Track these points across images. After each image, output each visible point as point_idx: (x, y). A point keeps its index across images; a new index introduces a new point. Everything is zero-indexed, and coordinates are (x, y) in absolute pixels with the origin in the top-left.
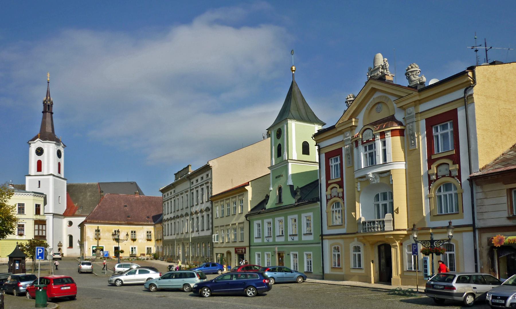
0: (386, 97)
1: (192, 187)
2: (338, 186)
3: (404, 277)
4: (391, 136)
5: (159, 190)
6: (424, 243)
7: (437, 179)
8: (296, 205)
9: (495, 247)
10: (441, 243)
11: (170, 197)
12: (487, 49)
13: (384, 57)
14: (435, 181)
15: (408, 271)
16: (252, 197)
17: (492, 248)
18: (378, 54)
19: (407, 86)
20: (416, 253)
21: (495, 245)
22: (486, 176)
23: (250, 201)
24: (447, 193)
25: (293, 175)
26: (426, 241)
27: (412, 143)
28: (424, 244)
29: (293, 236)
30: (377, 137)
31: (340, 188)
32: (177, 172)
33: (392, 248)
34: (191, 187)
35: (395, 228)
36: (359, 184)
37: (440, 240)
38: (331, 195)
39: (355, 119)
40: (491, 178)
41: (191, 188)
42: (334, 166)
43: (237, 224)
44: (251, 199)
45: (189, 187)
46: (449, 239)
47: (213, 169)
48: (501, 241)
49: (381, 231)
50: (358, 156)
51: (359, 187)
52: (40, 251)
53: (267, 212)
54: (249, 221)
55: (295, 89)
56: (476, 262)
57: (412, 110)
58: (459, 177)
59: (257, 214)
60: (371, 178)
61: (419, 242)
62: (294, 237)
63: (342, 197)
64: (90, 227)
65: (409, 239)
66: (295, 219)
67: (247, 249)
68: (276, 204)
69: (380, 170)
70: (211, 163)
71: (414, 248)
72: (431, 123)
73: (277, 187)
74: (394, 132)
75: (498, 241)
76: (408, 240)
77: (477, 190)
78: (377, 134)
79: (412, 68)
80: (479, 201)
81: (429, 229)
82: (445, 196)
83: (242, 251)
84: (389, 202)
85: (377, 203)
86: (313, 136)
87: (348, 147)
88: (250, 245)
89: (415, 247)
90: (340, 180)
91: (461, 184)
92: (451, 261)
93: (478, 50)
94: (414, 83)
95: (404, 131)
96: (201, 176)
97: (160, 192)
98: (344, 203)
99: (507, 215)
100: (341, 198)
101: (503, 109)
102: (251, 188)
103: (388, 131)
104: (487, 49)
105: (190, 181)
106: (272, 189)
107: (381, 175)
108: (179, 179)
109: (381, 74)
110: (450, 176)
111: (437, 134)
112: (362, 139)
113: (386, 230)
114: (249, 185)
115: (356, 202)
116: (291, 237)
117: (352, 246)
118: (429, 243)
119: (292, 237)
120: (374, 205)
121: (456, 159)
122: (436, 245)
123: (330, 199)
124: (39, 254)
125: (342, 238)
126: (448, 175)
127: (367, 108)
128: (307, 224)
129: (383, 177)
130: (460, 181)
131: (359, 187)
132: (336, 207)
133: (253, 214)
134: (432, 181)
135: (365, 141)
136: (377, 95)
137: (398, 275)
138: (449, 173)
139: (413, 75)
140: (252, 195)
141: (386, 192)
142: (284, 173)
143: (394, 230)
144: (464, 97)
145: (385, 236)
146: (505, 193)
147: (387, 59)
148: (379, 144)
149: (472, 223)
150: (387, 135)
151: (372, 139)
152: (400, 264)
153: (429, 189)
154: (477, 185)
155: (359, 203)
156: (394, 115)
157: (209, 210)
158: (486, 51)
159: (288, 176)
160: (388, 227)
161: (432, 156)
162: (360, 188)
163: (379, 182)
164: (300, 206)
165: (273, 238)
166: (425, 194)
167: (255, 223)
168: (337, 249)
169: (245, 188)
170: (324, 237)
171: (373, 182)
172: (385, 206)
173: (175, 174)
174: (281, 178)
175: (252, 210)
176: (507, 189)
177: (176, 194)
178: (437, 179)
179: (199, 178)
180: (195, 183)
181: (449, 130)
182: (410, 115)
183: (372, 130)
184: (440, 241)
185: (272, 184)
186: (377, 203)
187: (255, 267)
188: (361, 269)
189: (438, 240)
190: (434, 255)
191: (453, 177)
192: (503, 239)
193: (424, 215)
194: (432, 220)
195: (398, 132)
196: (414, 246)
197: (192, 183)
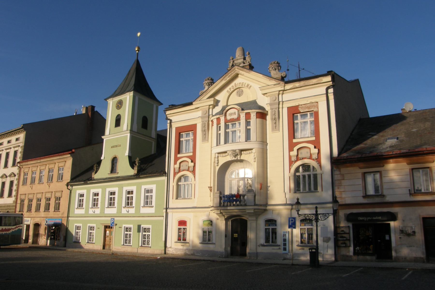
2: (189, 161)
10: (327, 216)
37: (326, 214)
50: (275, 127)
61: (302, 216)
62: (128, 209)
63: (316, 159)
64: (301, 132)
66: (83, 193)
71: (291, 222)
89: (112, 220)
90: (191, 154)
93: (287, 70)
96: (17, 136)
98: (195, 177)
99: (362, 195)
110: (310, 158)
119: (127, 209)
122: (321, 218)
123: (295, 161)
124: (292, 223)
125: (193, 212)
128: (80, 201)
146: (360, 175)
156: (256, 100)
157: (15, 176)
176: (362, 173)
181: (191, 137)
184: (326, 215)
188: (93, 243)
189: (323, 214)
196: (112, 219)
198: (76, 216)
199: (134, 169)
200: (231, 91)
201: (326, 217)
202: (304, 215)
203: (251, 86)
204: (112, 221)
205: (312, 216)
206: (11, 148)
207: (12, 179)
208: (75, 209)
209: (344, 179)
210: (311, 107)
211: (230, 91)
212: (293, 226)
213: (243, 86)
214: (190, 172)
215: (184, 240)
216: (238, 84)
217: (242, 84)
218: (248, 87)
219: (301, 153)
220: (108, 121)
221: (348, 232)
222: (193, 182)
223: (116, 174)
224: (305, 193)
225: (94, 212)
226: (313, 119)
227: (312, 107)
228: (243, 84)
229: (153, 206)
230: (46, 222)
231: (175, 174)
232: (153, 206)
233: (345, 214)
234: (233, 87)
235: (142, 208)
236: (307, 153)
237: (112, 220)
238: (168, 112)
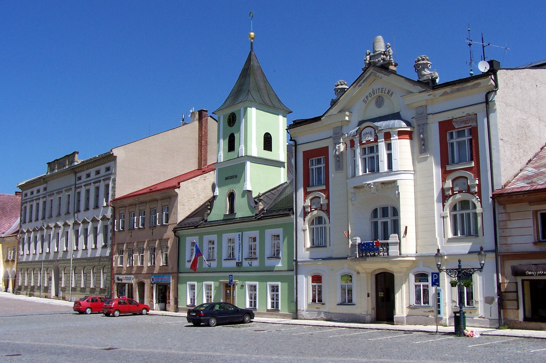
1: (78, 184)
4: (398, 139)
5: (17, 186)
6: (450, 272)
11: (36, 197)
12: (484, 46)
13: (385, 42)
18: (377, 37)
19: (416, 81)
20: (438, 284)
22: (510, 195)
24: (465, 212)
26: (452, 269)
28: (450, 274)
32: (53, 161)
34: (76, 184)
35: (402, 252)
37: (470, 269)
39: (349, 112)
40: (508, 198)
41: (77, 186)
42: (315, 168)
45: (74, 183)
46: (480, 267)
47: (118, 160)
52: (435, 276)
55: (254, 63)
59: (193, 227)
62: (251, 261)
70: (115, 152)
71: (434, 278)
80: (502, 224)
82: (462, 215)
84: (391, 220)
85: (375, 220)
86: (288, 128)
89: (231, 278)
94: (425, 78)
95: (412, 133)
97: (18, 188)
98: (329, 218)
99: (533, 241)
101: (520, 119)
104: (484, 46)
105: (76, 176)
108: (56, 171)
109: (382, 61)
111: (452, 141)
116: (248, 261)
118: (456, 272)
119: (250, 262)
120: (370, 222)
126: (466, 191)
132: (317, 223)
133: (181, 229)
134: (447, 196)
135: (365, 142)
138: (467, 188)
141: (388, 207)
147: (390, 43)
148: (382, 146)
152: (406, 298)
153: (444, 206)
156: (399, 112)
158: (483, 47)
164: (264, 219)
165: (217, 262)
172: (385, 224)
173: (47, 163)
176: (533, 211)
177: (47, 193)
179: (93, 171)
180: (84, 179)
186: (375, 220)
187: (434, 281)
189: (468, 269)
191: (472, 194)
196: (434, 275)
197: (80, 178)
198: (212, 271)
200: (368, 100)
202: (445, 270)
203: (392, 93)
204: (230, 279)
205: (455, 272)
206: (100, 181)
207: (105, 223)
208: (186, 262)
209: (509, 220)
210: (468, 120)
211: (367, 100)
213: (382, 93)
214: (323, 211)
215: (320, 301)
216: (376, 90)
217: (382, 91)
218: (389, 95)
220: (284, 136)
221: (515, 290)
222: (327, 225)
224: (314, 247)
225: (250, 264)
227: (470, 120)
228: (383, 91)
229: (257, 258)
230: (152, 281)
232: (257, 258)
233: (512, 266)
234: (371, 95)
235: (268, 259)
236: (464, 184)
237: (231, 278)
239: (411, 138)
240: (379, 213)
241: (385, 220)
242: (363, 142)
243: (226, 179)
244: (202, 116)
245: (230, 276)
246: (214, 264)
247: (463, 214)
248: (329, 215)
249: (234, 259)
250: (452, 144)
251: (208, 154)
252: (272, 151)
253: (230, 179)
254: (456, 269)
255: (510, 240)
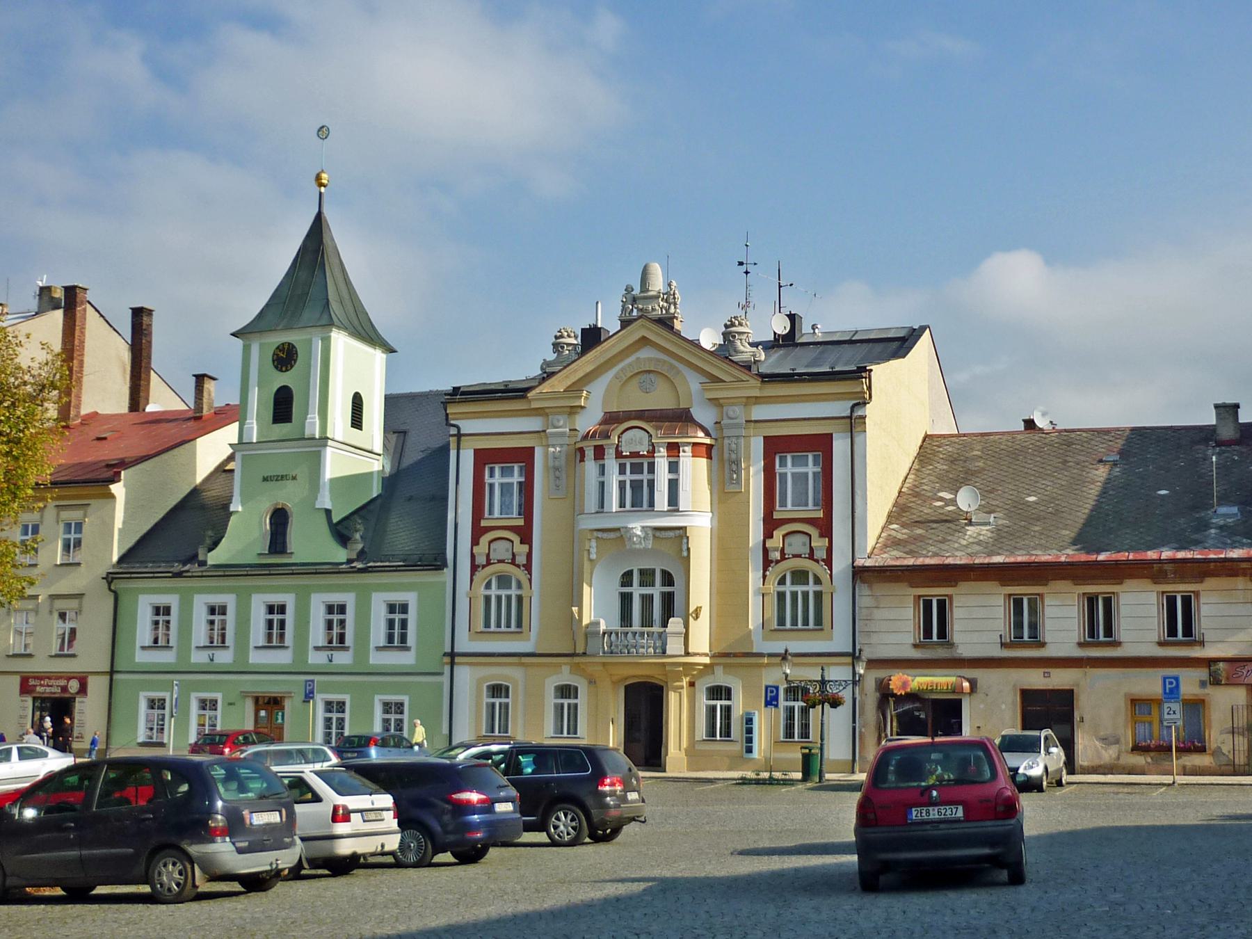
0: (672, 367)
2: (516, 539)
3: (693, 754)
4: (693, 456)
7: (783, 558)
8: (359, 569)
9: (894, 695)
14: (777, 562)
15: (704, 740)
16: (125, 517)
17: (885, 695)
21: (895, 692)
23: (119, 529)
25: (335, 482)
26: (810, 681)
27: (732, 479)
29: (332, 650)
30: (659, 452)
31: (522, 542)
33: (670, 692)
36: (594, 543)
38: (488, 555)
43: (40, 597)
44: (121, 526)
48: (905, 684)
49: (655, 656)
51: (593, 550)
53: (200, 574)
54: (115, 592)
56: (854, 721)
57: (737, 412)
58: (829, 562)
59: (170, 575)
60: (637, 536)
62: (214, 652)
65: (561, 672)
67: (97, 686)
68: (260, 554)
69: (661, 522)
71: (769, 694)
72: (775, 447)
73: (264, 507)
74: (697, 448)
75: (900, 684)
76: (712, 676)
77: (863, 590)
78: (660, 445)
79: (740, 324)
81: (761, 655)
83: (64, 689)
87: (560, 452)
88: (115, 669)
91: (831, 576)
92: (790, 724)
98: (530, 580)
99: (912, 641)
100: (522, 568)
102: (124, 490)
103: (688, 444)
106: (240, 509)
107: (658, 534)
112: (618, 446)
113: (668, 652)
114: (119, 481)
115: (585, 585)
117: (552, 683)
119: (329, 653)
121: (825, 528)
124: (771, 697)
126: (807, 556)
127: (618, 373)
129: (662, 538)
130: (831, 570)
131: (593, 550)
133: (129, 576)
134: (772, 562)
136: (646, 353)
137: (682, 749)
139: (741, 340)
140: (125, 513)
142: (302, 471)
143: (687, 654)
144: (850, 417)
145: (665, 666)
148: (662, 463)
149: (851, 651)
150: (684, 451)
151: (645, 453)
153: (764, 577)
154: (863, 581)
155: (591, 586)
158: (780, 287)
159: (321, 483)
160: (675, 647)
161: (482, 521)
162: (597, 553)
163: (650, 547)
166: (753, 586)
167: (144, 607)
168: (497, 690)
169: (110, 490)
170: (457, 660)
171: (637, 546)
174: (289, 483)
175: (122, 560)
178: (783, 558)
181: (811, 468)
182: (732, 421)
183: (648, 432)
185: (242, 494)
187: (768, 699)
189: (836, 681)
190: (827, 706)
192: (908, 681)
193: (751, 627)
194: (765, 638)
195: (704, 449)
196: (308, 683)
199: (348, 547)
201: (841, 688)
212: (775, 703)
219: (790, 545)
223: (286, 556)
226: (819, 470)
231: (474, 568)
233: (876, 679)
236: (804, 544)
238: (451, 410)
239: (709, 457)
240: (636, 579)
241: (647, 591)
242: (624, 454)
243: (265, 479)
244: (76, 302)
245: (306, 681)
246: (224, 657)
247: (797, 592)
248: (530, 574)
249: (283, 647)
250: (492, 486)
251: (83, 391)
252: (361, 430)
253: (277, 480)
254: (817, 681)
255: (875, 639)
